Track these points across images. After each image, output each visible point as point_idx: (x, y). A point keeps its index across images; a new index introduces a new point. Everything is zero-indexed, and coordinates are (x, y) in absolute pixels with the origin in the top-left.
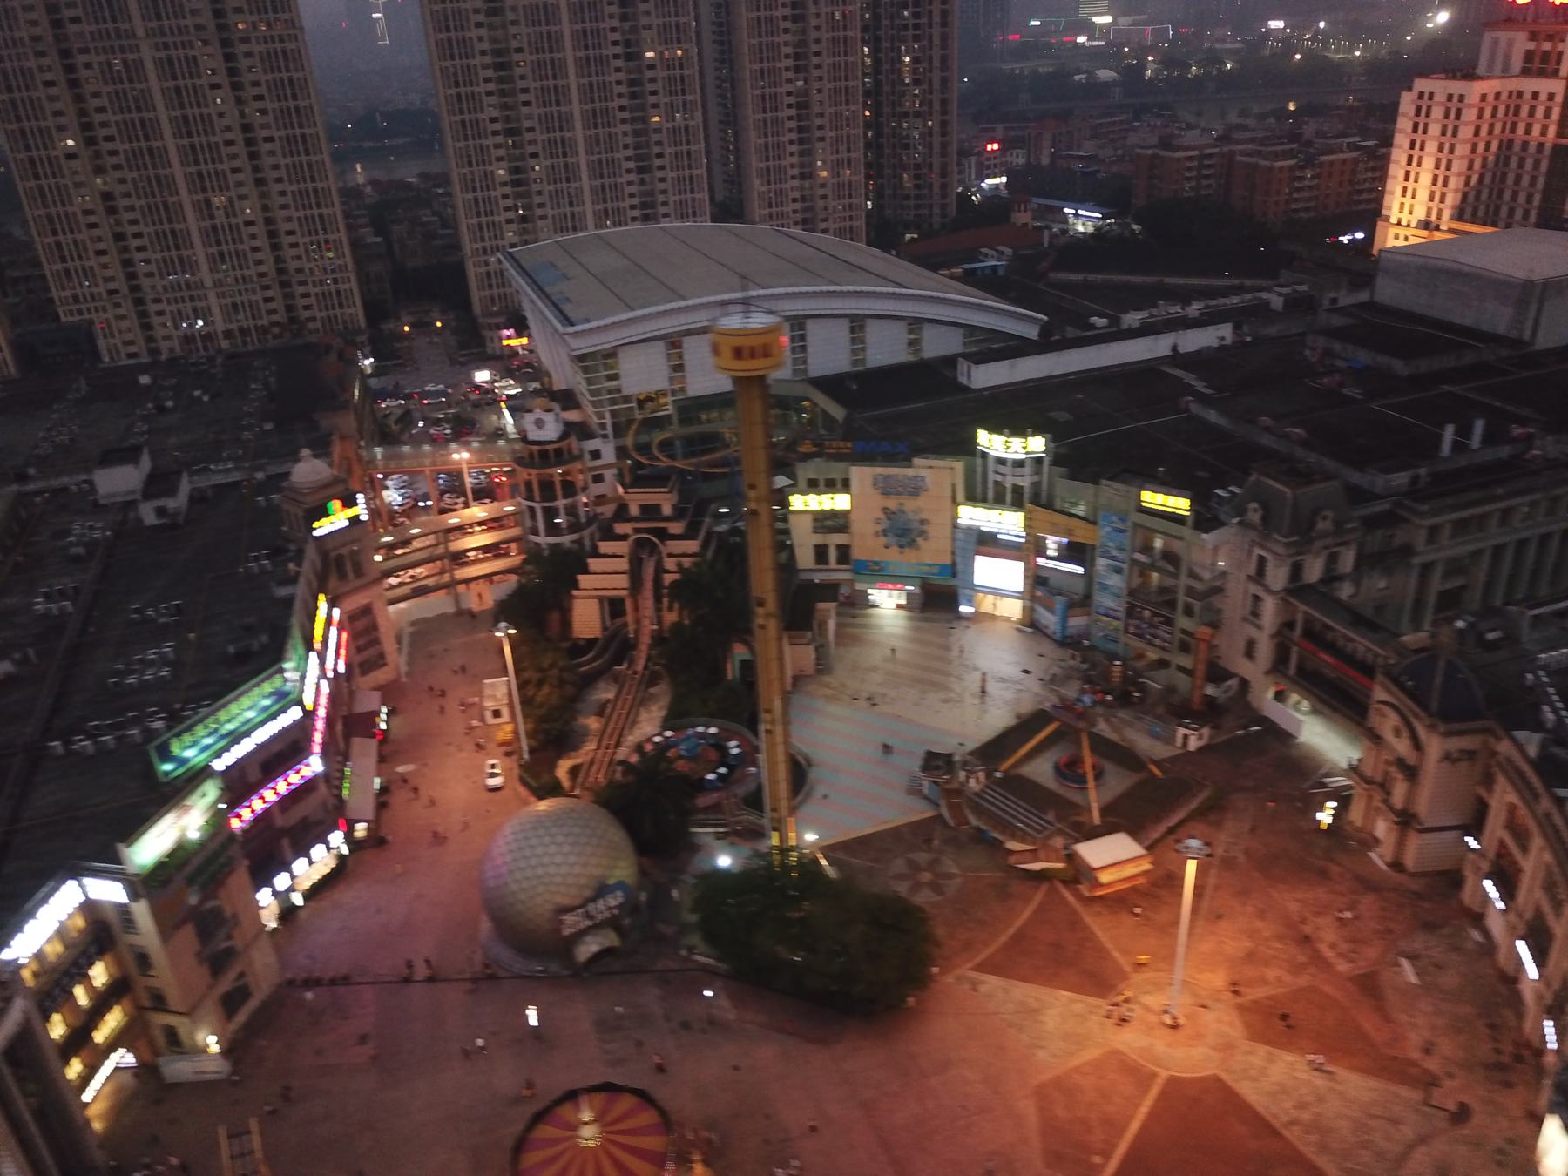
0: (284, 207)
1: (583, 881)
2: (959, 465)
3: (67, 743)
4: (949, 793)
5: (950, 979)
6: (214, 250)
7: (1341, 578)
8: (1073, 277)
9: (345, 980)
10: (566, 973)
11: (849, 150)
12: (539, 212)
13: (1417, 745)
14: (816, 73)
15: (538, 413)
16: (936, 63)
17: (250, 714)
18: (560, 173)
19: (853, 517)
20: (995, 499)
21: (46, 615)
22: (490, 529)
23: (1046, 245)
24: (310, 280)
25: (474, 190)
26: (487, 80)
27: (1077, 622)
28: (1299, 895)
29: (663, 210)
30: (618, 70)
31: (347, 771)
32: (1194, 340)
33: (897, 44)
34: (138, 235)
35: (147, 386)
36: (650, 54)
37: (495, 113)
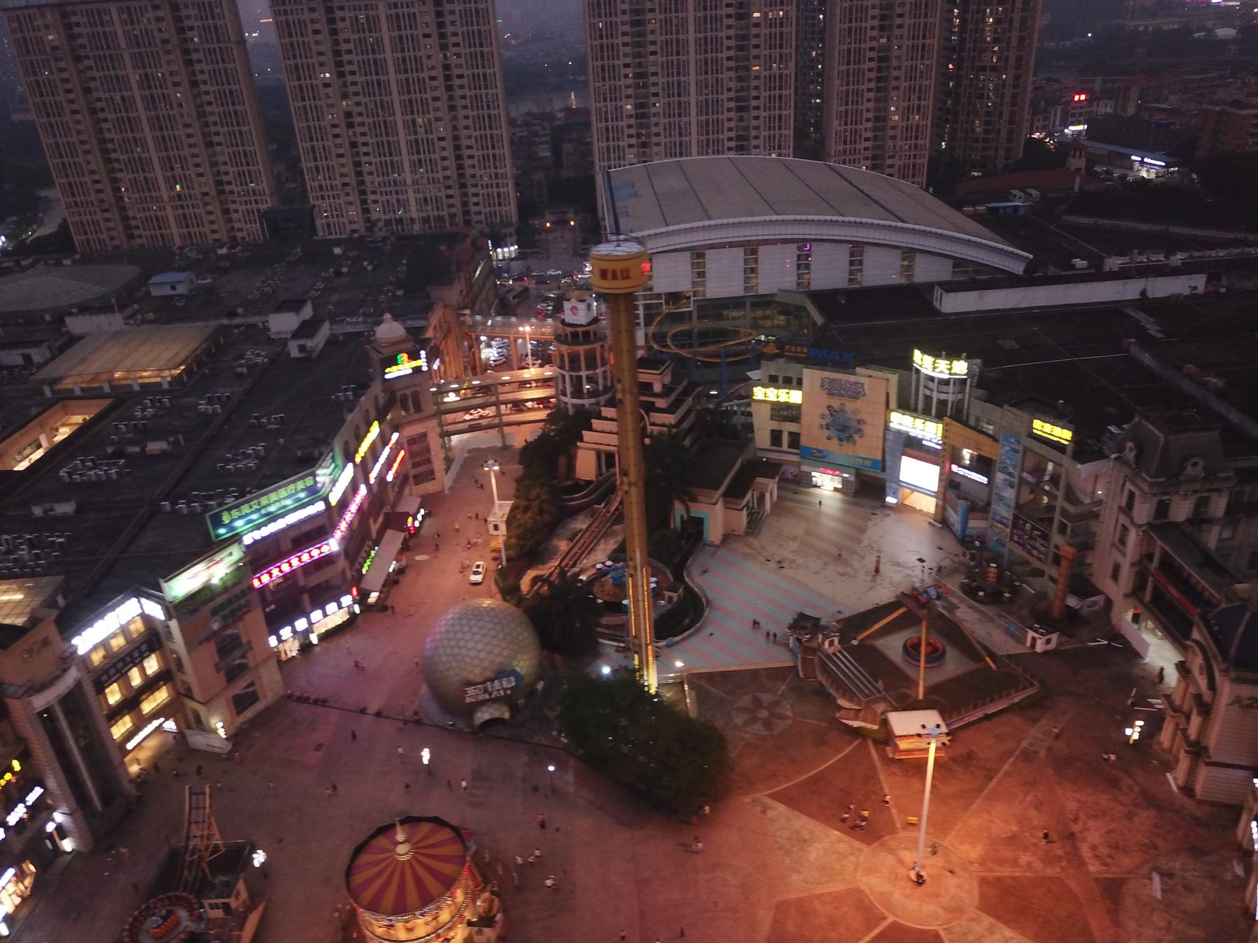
0: (467, 127)
1: (486, 664)
2: (894, 378)
3: (174, 504)
4: (807, 650)
5: (747, 799)
6: (415, 157)
7: (1210, 521)
8: (1085, 220)
9: (323, 703)
10: (467, 730)
11: (919, 99)
12: (655, 140)
13: (1212, 685)
14: (897, 32)
15: (574, 302)
16: (1016, 24)
17: (288, 502)
18: (674, 109)
19: (803, 410)
20: (925, 411)
21: (204, 414)
22: (543, 387)
23: (1076, 189)
24: (480, 184)
25: (607, 120)
26: (624, 34)
27: (975, 524)
28: (1078, 796)
29: (754, 142)
30: (729, 27)
31: (373, 553)
32: (1161, 288)
33: (983, 7)
34: (365, 144)
35: (338, 256)
36: (756, 15)
37: (628, 60)
